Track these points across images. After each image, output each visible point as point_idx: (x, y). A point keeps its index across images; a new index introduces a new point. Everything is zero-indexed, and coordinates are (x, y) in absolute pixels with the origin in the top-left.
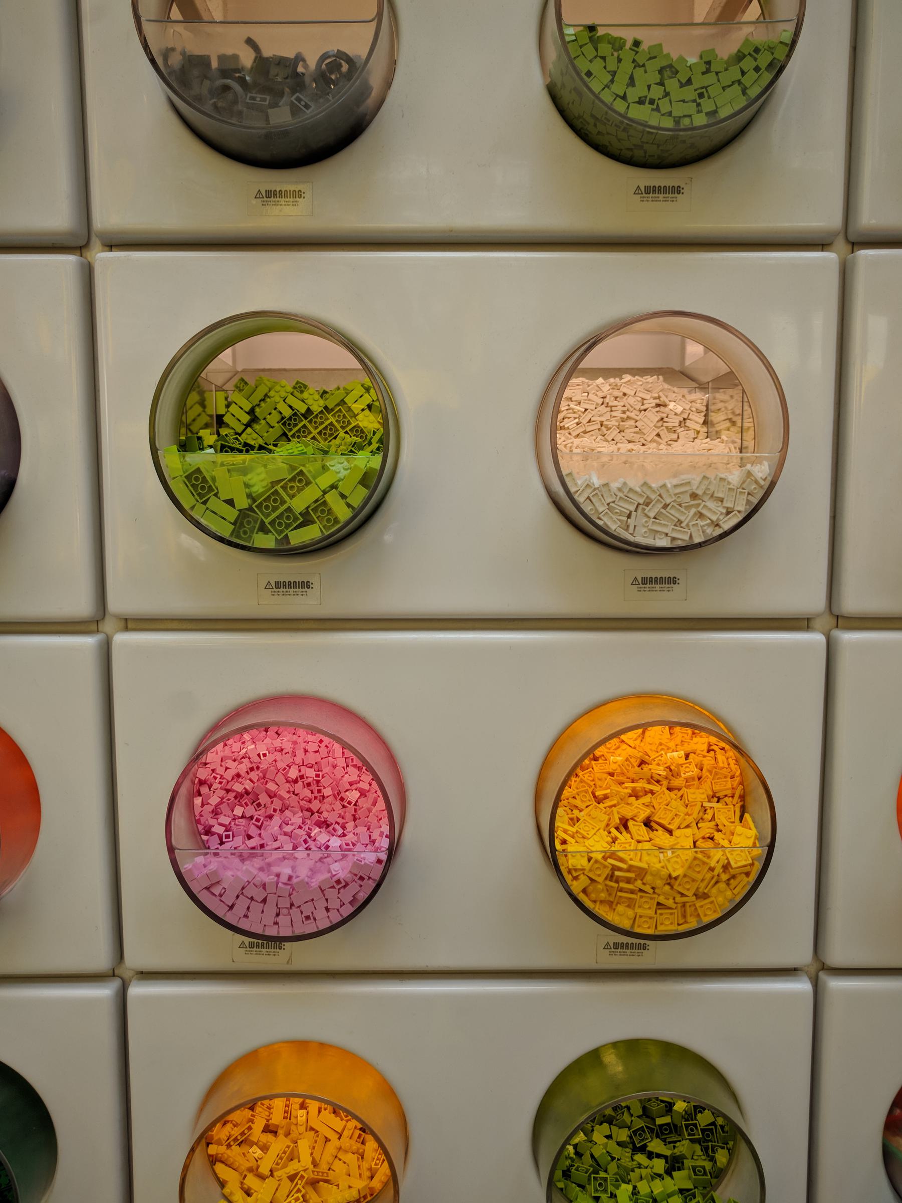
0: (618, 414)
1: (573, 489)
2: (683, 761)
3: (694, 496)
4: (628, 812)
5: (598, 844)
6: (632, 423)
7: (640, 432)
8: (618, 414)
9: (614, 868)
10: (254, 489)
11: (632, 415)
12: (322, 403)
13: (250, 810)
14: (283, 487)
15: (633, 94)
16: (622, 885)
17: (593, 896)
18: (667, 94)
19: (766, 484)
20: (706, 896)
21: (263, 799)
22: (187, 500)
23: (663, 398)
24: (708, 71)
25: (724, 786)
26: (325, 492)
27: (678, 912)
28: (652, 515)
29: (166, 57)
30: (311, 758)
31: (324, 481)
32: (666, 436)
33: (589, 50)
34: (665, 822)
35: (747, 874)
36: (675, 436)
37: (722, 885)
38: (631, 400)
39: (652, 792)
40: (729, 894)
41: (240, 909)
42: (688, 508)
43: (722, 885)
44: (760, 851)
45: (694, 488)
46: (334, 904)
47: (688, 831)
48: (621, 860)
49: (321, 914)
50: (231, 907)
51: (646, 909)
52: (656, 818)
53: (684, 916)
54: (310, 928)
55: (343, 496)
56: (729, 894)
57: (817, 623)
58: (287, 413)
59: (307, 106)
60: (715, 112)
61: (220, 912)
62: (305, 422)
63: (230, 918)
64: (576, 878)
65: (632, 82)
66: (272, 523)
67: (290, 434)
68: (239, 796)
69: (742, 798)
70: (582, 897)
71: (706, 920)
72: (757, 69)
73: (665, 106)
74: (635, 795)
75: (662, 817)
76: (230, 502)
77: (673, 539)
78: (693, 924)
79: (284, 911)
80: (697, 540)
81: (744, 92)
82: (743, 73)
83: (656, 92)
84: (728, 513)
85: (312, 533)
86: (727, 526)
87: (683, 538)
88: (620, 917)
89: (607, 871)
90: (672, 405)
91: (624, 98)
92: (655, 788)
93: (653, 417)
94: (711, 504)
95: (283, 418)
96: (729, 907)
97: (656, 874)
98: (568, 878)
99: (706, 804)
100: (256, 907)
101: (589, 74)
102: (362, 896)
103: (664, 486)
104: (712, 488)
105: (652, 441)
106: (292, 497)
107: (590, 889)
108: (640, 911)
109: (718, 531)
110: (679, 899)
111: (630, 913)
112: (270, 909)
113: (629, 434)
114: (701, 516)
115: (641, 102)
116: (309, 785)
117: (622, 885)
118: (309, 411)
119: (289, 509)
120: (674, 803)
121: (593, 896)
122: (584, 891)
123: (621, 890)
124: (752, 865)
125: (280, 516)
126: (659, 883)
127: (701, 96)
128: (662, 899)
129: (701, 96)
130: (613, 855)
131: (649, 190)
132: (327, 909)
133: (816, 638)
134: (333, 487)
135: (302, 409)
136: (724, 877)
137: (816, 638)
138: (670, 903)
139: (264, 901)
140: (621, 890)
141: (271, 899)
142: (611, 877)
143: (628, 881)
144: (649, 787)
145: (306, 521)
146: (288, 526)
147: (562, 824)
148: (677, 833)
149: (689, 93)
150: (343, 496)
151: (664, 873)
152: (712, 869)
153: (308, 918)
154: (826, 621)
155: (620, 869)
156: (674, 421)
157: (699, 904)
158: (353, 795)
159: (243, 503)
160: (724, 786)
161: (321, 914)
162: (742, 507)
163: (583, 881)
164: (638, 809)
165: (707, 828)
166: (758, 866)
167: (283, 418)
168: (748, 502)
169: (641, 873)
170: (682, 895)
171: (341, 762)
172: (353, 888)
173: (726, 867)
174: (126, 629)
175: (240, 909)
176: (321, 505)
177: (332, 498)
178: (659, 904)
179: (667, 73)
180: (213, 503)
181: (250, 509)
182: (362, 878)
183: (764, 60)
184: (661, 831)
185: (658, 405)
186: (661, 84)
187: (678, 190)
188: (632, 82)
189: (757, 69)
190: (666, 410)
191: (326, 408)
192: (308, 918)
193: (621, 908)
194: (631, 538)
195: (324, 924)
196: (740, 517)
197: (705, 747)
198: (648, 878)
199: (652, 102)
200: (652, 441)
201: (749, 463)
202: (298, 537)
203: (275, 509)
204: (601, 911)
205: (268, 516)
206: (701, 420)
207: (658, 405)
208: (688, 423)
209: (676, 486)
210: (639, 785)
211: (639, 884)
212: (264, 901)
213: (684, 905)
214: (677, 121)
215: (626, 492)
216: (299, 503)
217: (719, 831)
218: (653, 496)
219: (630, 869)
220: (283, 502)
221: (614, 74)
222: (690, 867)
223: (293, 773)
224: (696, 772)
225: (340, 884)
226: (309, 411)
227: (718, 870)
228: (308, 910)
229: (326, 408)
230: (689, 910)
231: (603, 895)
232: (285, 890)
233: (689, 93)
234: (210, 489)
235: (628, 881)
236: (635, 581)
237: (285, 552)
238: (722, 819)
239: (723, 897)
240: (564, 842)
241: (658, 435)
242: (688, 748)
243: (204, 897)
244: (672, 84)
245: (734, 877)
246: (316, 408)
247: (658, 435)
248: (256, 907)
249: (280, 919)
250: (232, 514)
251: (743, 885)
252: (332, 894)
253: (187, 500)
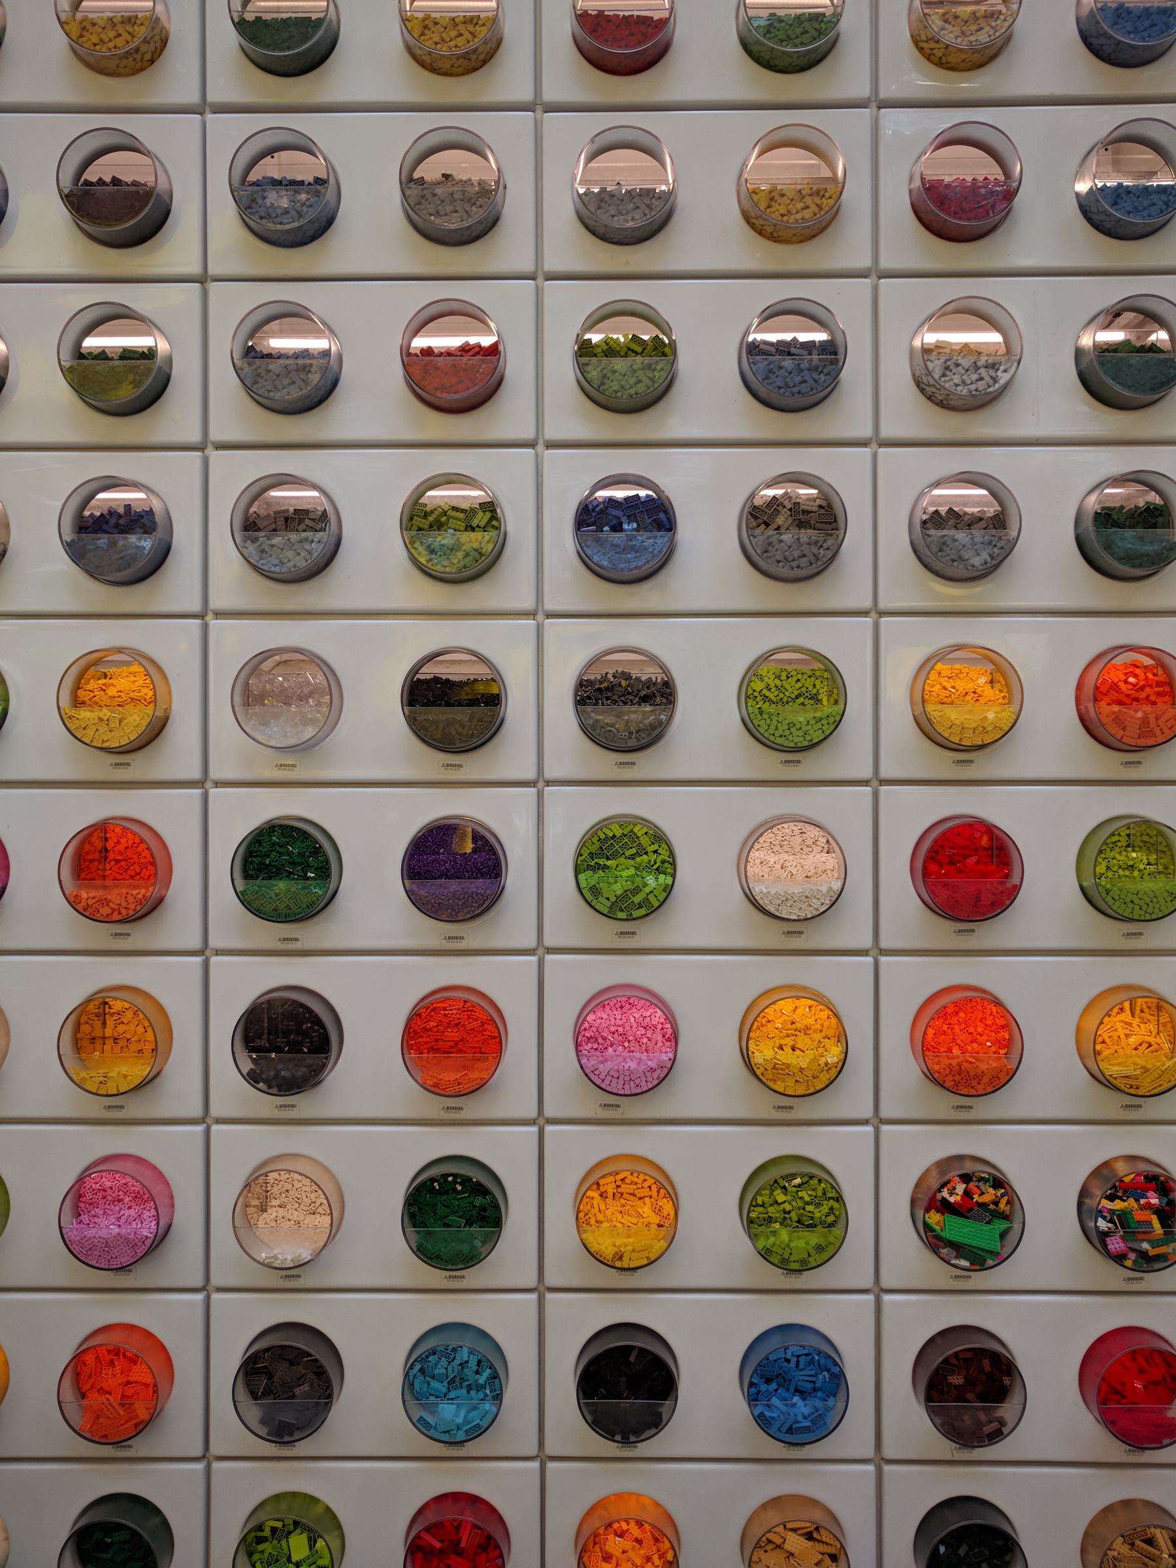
0: (780, 838)
1: (754, 894)
2: (814, 1022)
3: (807, 897)
4: (783, 1042)
5: (769, 1053)
6: (787, 842)
7: (792, 847)
8: (780, 838)
9: (776, 1064)
10: (617, 893)
11: (787, 838)
12: (621, 831)
13: (595, 1046)
14: (630, 892)
15: (777, 734)
16: (779, 1071)
17: (766, 1077)
18: (791, 733)
19: (838, 893)
20: (818, 1077)
21: (600, 1040)
22: (589, 897)
23: (804, 830)
24: (808, 724)
25: (831, 1033)
26: (648, 895)
27: (805, 1085)
28: (789, 905)
29: (240, 199)
30: (620, 1023)
31: (647, 890)
32: (806, 850)
33: (759, 717)
34: (801, 1047)
35: (836, 1067)
36: (811, 849)
37: (825, 1072)
38: (787, 831)
39: (796, 1036)
40: (828, 1076)
41: (607, 1082)
42: (805, 902)
43: (825, 1072)
44: (842, 1057)
45: (807, 893)
46: (650, 1079)
47: (812, 1052)
48: (779, 1060)
49: (643, 1084)
50: (603, 1081)
51: (790, 1082)
52: (797, 1046)
53: (808, 1086)
54: (639, 1090)
55: (656, 896)
56: (828, 1076)
57: (871, 953)
58: (603, 836)
59: (643, 738)
60: (811, 740)
61: (598, 1082)
62: (612, 841)
63: (603, 1086)
64: (758, 1068)
65: (777, 729)
66: (625, 908)
67: (604, 848)
68: (589, 1039)
69: (838, 1037)
70: (761, 1077)
71: (818, 1088)
72: (828, 724)
73: (790, 738)
74: (788, 1036)
75: (799, 1045)
76: (608, 899)
77: (798, 916)
78: (812, 1090)
79: (627, 1082)
80: (809, 916)
81: (823, 732)
82: (823, 725)
83: (787, 733)
84: (822, 904)
85: (642, 912)
86: (822, 910)
87: (803, 915)
88: (779, 1087)
89: (772, 1065)
90: (809, 833)
91: (773, 735)
92: (798, 1033)
93: (798, 839)
94: (814, 901)
95: (600, 839)
96: (828, 1082)
97: (795, 1067)
98: (755, 1068)
99: (822, 1040)
100: (615, 1081)
101: (759, 726)
102: (662, 1076)
103: (794, 893)
104: (815, 894)
105: (798, 852)
106: (634, 896)
107: (765, 1073)
108: (788, 1084)
109: (818, 913)
110: (805, 1078)
111: (783, 1085)
112: (621, 1082)
113: (786, 848)
114: (810, 906)
115: (781, 736)
116: (621, 1035)
117: (779, 1071)
118: (614, 836)
119: (632, 902)
120: (806, 1040)
121: (766, 1077)
122: (762, 1074)
123: (779, 1074)
124: (838, 1063)
125: (629, 905)
126: (796, 1071)
127: (805, 734)
128: (797, 1079)
129: (805, 734)
130: (775, 1058)
131: (786, 762)
132: (646, 1082)
133: (870, 959)
134: (651, 892)
135: (611, 834)
136: (826, 1068)
137: (870, 959)
138: (801, 1080)
139: (618, 1078)
140: (779, 1074)
141: (622, 1077)
142: (774, 1068)
143: (782, 1069)
144: (794, 1033)
145: (640, 906)
146: (632, 909)
147: (752, 1046)
148: (807, 1052)
149: (800, 733)
150: (656, 896)
151: (798, 1066)
152: (819, 1065)
153: (637, 1086)
154: (874, 952)
155: (778, 1064)
156: (809, 842)
157: (814, 1081)
158: (645, 1040)
159: (613, 899)
160: (831, 1033)
161: (643, 1084)
162: (828, 902)
163: (762, 1069)
164: (789, 1042)
165: (820, 1050)
166: (841, 1064)
167: (600, 839)
168: (830, 900)
169: (788, 1066)
170: (807, 1076)
171: (635, 1025)
172: (658, 1071)
173: (827, 1064)
174: (217, 955)
175: (607, 1082)
176: (646, 899)
177: (651, 897)
178: (796, 1081)
179: (791, 725)
180: (600, 899)
181: (616, 901)
182: (662, 1067)
183: (831, 720)
184: (798, 1051)
185: (801, 833)
186: (789, 729)
187: (799, 762)
188: (777, 729)
189: (828, 724)
190: (806, 835)
191: (623, 834)
192: (637, 1086)
193: (779, 1083)
194: (780, 915)
195: (645, 1089)
196: (827, 907)
197: (826, 1016)
198: (791, 1068)
199: (785, 736)
200: (798, 852)
201: (473, 1182)
202: (636, 914)
203: (627, 901)
204: (770, 1084)
205: (623, 904)
206: (825, 841)
207: (801, 833)
208: (818, 843)
209: (799, 893)
210: (790, 1032)
211: (787, 1071)
212: (618, 1078)
213: (808, 1082)
214: (796, 744)
215: (777, 896)
216: (637, 899)
217: (826, 1051)
218: (789, 897)
219: (783, 1064)
220: (630, 898)
221: (769, 726)
222: (810, 1064)
223: (613, 1029)
224: (820, 1027)
225: (652, 1070)
226: (614, 836)
227: (823, 1065)
228: (637, 1082)
229: (623, 834)
230: (810, 1084)
231: (771, 1076)
232: (627, 1073)
233: (800, 733)
234: (600, 893)
235: (782, 1069)
236: (784, 933)
237: (630, 919)
238: (827, 1046)
239: (825, 1078)
240: (753, 1053)
241: (802, 849)
242: (817, 1017)
243: (591, 1075)
244: (793, 730)
245: (830, 1069)
246: (618, 835)
247: (802, 849)
248: (615, 1081)
249: (625, 1087)
250: (608, 904)
251: (834, 1072)
252: (648, 1074)
253: (589, 897)
